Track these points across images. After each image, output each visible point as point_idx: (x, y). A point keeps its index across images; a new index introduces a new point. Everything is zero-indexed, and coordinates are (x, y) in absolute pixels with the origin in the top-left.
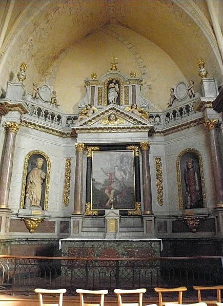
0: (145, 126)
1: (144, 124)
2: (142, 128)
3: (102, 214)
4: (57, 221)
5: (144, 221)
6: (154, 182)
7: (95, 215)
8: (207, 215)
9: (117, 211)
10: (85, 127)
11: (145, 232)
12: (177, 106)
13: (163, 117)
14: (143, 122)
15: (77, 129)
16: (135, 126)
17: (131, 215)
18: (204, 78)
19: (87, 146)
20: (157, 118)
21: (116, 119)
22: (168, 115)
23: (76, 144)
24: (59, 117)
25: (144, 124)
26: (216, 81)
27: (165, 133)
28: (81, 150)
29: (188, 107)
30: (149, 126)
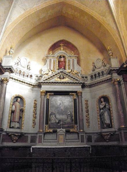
0: (80, 82)
1: (79, 81)
2: (79, 83)
3: (55, 132)
4: (29, 136)
5: (80, 136)
6: (85, 114)
7: (51, 132)
8: (115, 132)
9: (64, 130)
10: (46, 81)
11: (80, 142)
12: (97, 71)
13: (89, 78)
14: (79, 80)
15: (42, 82)
16: (75, 82)
17: (72, 132)
18: (111, 57)
19: (47, 92)
20: (86, 79)
21: (64, 78)
22: (92, 77)
23: (41, 91)
24: (31, 76)
25: (79, 81)
26: (118, 59)
27: (90, 86)
28: (43, 94)
29: (103, 72)
30: (82, 82)
